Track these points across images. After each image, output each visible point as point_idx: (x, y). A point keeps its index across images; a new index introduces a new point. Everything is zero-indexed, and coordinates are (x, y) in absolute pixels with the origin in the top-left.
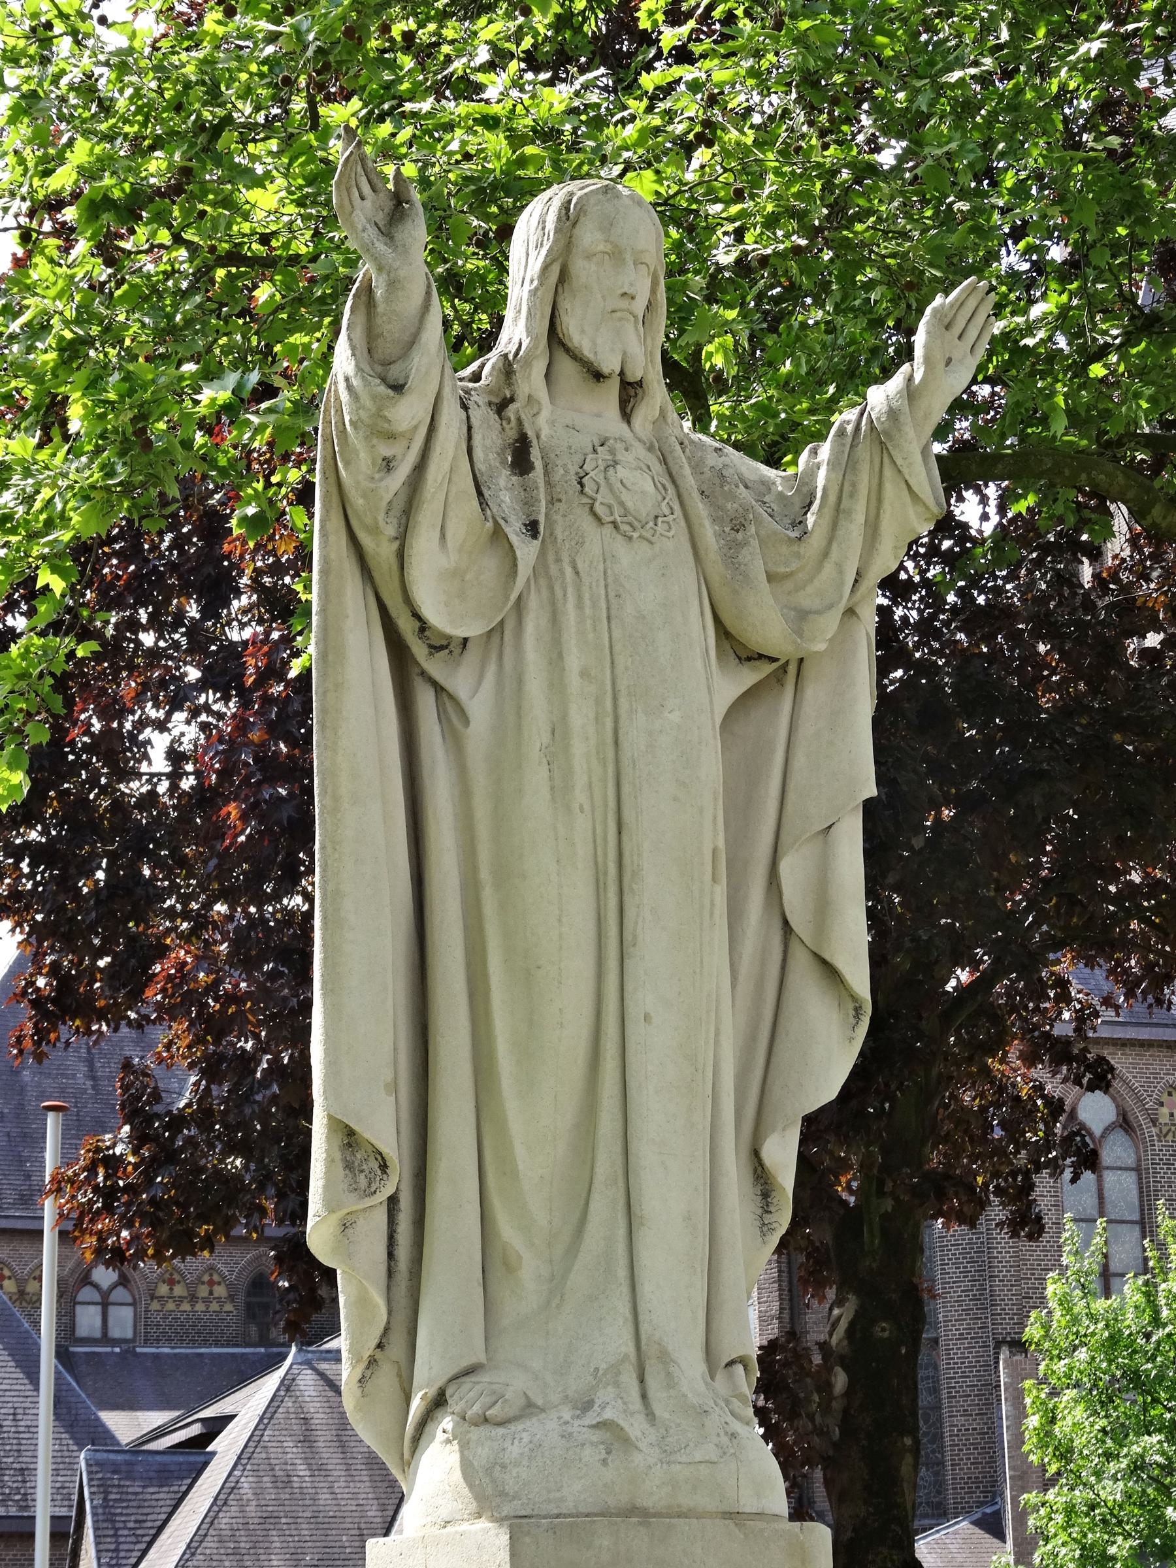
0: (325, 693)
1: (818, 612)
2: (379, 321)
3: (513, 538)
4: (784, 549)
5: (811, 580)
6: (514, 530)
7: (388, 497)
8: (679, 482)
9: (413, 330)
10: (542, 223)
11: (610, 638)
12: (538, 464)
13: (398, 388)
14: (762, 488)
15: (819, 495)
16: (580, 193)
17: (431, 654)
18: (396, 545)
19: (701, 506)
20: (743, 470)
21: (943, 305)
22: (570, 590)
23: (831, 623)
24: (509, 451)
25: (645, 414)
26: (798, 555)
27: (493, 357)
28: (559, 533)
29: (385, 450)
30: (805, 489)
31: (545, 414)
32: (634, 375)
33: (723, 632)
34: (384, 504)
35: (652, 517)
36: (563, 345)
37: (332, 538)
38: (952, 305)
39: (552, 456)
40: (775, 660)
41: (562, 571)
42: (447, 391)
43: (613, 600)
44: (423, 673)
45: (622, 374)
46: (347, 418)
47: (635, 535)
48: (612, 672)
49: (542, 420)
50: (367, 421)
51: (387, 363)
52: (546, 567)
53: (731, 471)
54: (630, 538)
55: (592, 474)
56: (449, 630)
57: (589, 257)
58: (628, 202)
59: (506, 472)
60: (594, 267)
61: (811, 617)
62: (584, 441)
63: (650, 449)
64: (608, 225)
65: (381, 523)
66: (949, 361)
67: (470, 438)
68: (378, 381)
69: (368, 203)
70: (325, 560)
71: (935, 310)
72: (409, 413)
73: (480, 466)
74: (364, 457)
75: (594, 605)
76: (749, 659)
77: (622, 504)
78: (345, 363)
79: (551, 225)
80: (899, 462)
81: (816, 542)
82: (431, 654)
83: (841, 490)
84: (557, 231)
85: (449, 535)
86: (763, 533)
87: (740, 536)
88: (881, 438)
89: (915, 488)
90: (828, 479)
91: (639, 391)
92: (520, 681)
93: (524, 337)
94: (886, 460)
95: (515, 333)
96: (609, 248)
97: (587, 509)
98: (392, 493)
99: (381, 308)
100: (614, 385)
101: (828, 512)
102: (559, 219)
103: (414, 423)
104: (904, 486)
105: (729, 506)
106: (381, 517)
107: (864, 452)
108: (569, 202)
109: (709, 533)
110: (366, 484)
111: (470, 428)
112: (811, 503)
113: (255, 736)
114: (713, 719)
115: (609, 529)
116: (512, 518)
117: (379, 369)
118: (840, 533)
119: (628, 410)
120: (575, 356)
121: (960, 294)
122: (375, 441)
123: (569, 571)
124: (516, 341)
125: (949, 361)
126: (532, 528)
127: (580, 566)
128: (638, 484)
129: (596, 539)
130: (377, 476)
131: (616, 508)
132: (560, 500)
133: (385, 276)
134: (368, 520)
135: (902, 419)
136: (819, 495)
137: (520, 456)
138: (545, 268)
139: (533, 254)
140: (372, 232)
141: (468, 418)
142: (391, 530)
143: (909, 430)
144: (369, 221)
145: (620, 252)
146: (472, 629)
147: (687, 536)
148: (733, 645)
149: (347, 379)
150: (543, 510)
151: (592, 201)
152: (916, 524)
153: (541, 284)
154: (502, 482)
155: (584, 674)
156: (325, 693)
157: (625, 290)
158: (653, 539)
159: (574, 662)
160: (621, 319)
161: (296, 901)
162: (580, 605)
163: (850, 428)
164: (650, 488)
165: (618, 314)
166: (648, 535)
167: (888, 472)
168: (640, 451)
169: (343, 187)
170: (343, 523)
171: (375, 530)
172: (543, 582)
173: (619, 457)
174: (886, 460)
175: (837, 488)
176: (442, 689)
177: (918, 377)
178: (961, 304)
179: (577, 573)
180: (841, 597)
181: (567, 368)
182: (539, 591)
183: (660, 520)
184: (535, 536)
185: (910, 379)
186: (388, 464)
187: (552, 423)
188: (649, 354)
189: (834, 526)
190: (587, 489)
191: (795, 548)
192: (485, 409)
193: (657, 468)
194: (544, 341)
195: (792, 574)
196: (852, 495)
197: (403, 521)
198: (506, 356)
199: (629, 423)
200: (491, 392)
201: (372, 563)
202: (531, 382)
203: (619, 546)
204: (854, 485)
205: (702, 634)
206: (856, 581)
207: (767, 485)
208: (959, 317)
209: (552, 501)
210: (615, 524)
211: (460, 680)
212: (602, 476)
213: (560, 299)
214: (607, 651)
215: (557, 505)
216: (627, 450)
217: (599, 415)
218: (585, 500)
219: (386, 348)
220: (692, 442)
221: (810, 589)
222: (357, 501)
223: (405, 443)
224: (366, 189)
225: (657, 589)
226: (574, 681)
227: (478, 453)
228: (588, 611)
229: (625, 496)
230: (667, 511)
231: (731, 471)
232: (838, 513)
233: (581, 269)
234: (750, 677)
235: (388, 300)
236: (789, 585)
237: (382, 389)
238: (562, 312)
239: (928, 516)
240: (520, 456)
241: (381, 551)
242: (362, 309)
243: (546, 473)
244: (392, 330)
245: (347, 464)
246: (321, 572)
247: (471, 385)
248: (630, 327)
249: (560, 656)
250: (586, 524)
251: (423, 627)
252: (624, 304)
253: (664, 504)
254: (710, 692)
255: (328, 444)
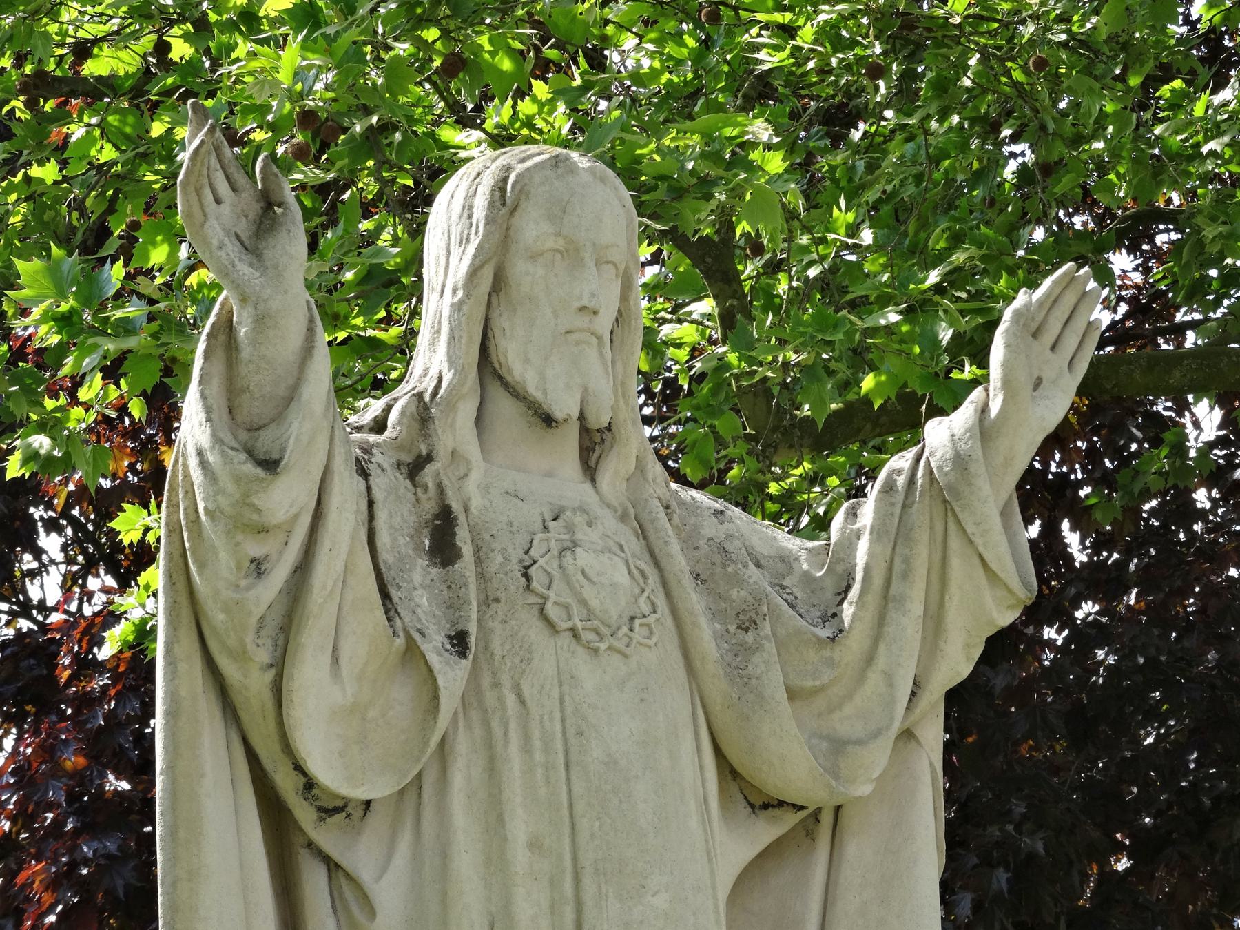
0: (174, 884)
1: (860, 742)
2: (243, 370)
3: (434, 660)
4: (812, 655)
5: (849, 696)
6: (434, 647)
7: (258, 611)
8: (664, 563)
9: (291, 382)
10: (468, 208)
11: (570, 791)
12: (467, 550)
13: (270, 465)
14: (780, 567)
15: (859, 576)
16: (520, 168)
17: (321, 819)
18: (270, 675)
19: (694, 597)
20: (754, 540)
21: (1028, 306)
22: (513, 726)
23: (878, 756)
24: (426, 532)
25: (614, 470)
26: (831, 663)
27: (402, 396)
28: (497, 646)
29: (254, 549)
30: (840, 568)
31: (475, 476)
32: (600, 418)
33: (728, 771)
34: (254, 620)
35: (626, 619)
36: (500, 378)
37: (182, 667)
38: (1041, 303)
39: (487, 537)
40: (802, 808)
41: (501, 699)
42: (339, 452)
43: (573, 740)
44: (310, 844)
45: (582, 417)
46: (201, 506)
47: (603, 646)
48: (573, 842)
49: (472, 486)
50: (228, 510)
51: (255, 429)
52: (479, 692)
53: (737, 543)
54: (596, 651)
55: (542, 561)
56: (345, 790)
57: (533, 257)
58: (586, 178)
59: (423, 562)
60: (541, 272)
61: (850, 748)
62: (531, 514)
63: (623, 518)
64: (558, 212)
65: (250, 647)
66: (1038, 383)
67: (371, 517)
68: (243, 456)
69: (226, 209)
70: (172, 696)
71: (1017, 314)
72: (287, 497)
73: (385, 556)
74: (224, 559)
75: (547, 748)
76: (765, 806)
77: (583, 602)
78: (197, 431)
79: (479, 213)
80: (970, 529)
81: (855, 644)
82: (321, 819)
83: (890, 569)
84: (489, 221)
85: (344, 660)
86: (781, 632)
87: (749, 638)
88: (944, 494)
89: (993, 565)
90: (871, 554)
91: (607, 436)
92: (445, 855)
93: (445, 370)
94: (952, 526)
95: (432, 362)
96: (560, 244)
97: (535, 611)
98: (264, 606)
99: (246, 352)
100: (570, 438)
101: (873, 600)
102: (491, 204)
103: (294, 511)
104: (977, 561)
105: (734, 594)
106: (249, 638)
107: (921, 514)
108: (505, 180)
109: (706, 634)
110: (227, 594)
111: (371, 504)
112: (848, 588)
113: (72, 760)
114: (715, 898)
115: (566, 639)
116: (432, 630)
117: (244, 435)
118: (890, 629)
119: (592, 463)
120: (516, 393)
121: (1052, 288)
122: (240, 537)
123: (511, 700)
124: (434, 373)
125: (1038, 383)
126: (459, 642)
127: (526, 692)
128: (605, 572)
129: (549, 655)
130: (243, 583)
131: (575, 609)
132: (497, 600)
133: (250, 309)
134: (232, 642)
135: (973, 468)
136: (859, 576)
137: (442, 539)
138: (473, 273)
139: (456, 252)
140: (232, 248)
141: (369, 489)
142: (263, 655)
143: (983, 485)
144: (227, 232)
145: (577, 250)
146: (377, 788)
147: (676, 640)
148: (743, 791)
149: (200, 453)
150: (474, 616)
151: (537, 179)
152: (995, 614)
153: (468, 295)
154: (417, 577)
155: (534, 845)
156: (174, 884)
157: (585, 302)
158: (627, 651)
159: (519, 828)
160: (578, 343)
161: (148, 829)
162: (527, 748)
163: (901, 481)
164: (622, 577)
165: (575, 336)
166: (620, 645)
167: (955, 543)
168: (609, 522)
169: (191, 189)
170: (196, 645)
171: (241, 656)
172: (475, 715)
173: (579, 536)
174: (952, 526)
175: (884, 565)
176: (338, 866)
177: (995, 407)
178: (1052, 301)
179: (523, 702)
180: (892, 719)
181: (504, 407)
182: (469, 727)
183: (637, 622)
184: (463, 654)
185: (984, 410)
186: (258, 568)
187: (485, 489)
188: (620, 388)
189: (881, 620)
190: (534, 584)
191: (827, 653)
192: (392, 474)
193: (633, 545)
194: (473, 373)
195: (823, 688)
196: (905, 576)
197: (281, 642)
198: (420, 395)
199: (593, 481)
200: (400, 448)
201: (238, 700)
202: (456, 431)
203: (580, 662)
204: (907, 561)
205: (697, 774)
206: (913, 694)
207: (786, 561)
208: (1051, 319)
209: (487, 601)
210: (574, 632)
211: (361, 854)
212: (555, 564)
213: (494, 315)
214: (565, 812)
215: (494, 606)
216: (590, 524)
217: (549, 474)
218: (533, 599)
219: (251, 408)
220: (682, 503)
221: (848, 709)
222: (216, 617)
223: (282, 537)
224: (223, 188)
225: (632, 719)
226: (520, 857)
227: (384, 539)
228: (538, 756)
229: (588, 593)
230: (646, 609)
231: (737, 543)
232: (886, 600)
233: (523, 272)
234: (766, 831)
235: (254, 343)
236: (820, 703)
237: (249, 468)
238: (498, 333)
239: (1012, 601)
240: (442, 539)
241: (251, 683)
242: (220, 355)
243: (478, 561)
244: (261, 381)
245: (201, 566)
246: (169, 714)
247: (373, 438)
248: (592, 354)
249: (500, 820)
250: (534, 631)
251: (310, 785)
252: (582, 321)
253: (642, 599)
254: (710, 860)
255: (175, 536)
